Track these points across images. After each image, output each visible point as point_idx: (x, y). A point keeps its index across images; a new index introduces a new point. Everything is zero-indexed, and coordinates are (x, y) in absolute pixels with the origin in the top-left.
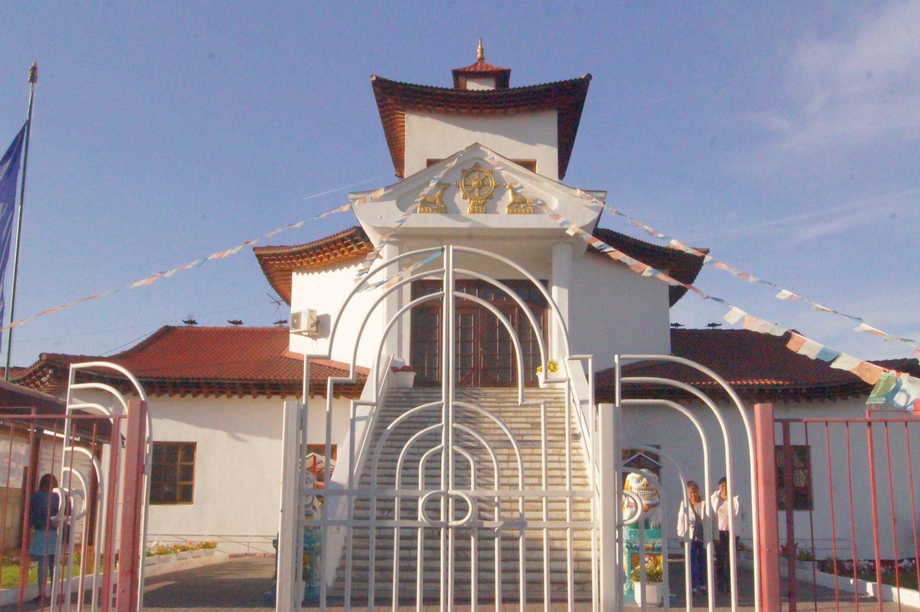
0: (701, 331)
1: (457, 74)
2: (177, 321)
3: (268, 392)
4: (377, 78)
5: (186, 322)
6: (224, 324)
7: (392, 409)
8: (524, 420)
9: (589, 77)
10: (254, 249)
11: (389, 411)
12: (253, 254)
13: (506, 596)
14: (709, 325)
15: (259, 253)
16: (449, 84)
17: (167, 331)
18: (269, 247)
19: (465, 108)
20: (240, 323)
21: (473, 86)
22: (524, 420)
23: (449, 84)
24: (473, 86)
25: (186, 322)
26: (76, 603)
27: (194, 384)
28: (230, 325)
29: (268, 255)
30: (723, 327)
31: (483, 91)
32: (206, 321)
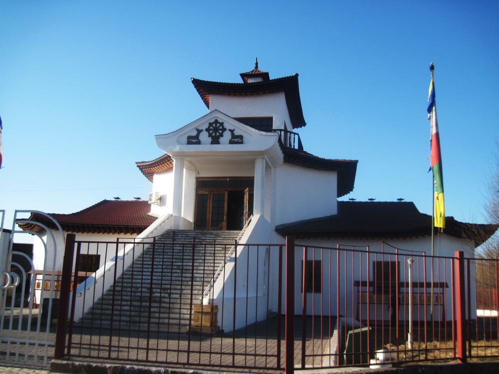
0: (346, 202)
1: (242, 75)
2: (111, 198)
3: (113, 231)
4: (194, 79)
5: (115, 198)
6: (366, 200)
7: (186, 240)
10: (136, 163)
11: (160, 241)
12: (136, 165)
13: (23, 357)
14: (369, 200)
15: (139, 165)
16: (241, 81)
17: (105, 203)
18: (143, 162)
19: (238, 92)
20: (139, 198)
21: (250, 81)
23: (241, 81)
24: (250, 81)
25: (115, 198)
26: (408, 287)
27: (131, 228)
29: (143, 166)
30: (356, 201)
31: (257, 82)
32: (124, 198)
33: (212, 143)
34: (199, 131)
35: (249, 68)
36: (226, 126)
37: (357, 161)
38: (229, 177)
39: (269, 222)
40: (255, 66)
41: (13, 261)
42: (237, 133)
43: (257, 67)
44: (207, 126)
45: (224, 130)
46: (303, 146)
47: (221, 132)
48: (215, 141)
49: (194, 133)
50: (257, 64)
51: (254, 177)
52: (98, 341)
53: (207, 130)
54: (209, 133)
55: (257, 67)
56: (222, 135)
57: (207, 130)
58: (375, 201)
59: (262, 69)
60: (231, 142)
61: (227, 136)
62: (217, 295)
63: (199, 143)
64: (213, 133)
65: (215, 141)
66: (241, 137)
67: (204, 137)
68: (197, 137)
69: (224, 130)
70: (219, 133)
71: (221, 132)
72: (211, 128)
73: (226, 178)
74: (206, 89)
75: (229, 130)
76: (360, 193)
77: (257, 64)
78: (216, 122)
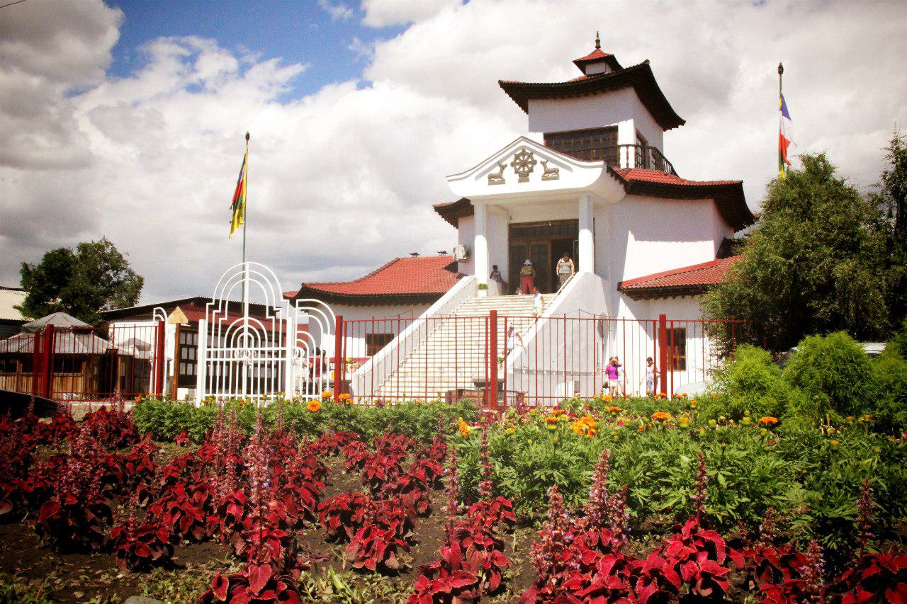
20: (445, 252)
33: (520, 181)
34: (503, 168)
35: (586, 51)
36: (535, 157)
37: (647, 61)
38: (552, 222)
39: (630, 233)
40: (595, 44)
41: (298, 330)
42: (550, 166)
43: (598, 47)
45: (534, 163)
46: (686, 244)
47: (518, 161)
48: (524, 177)
49: (497, 170)
50: (598, 41)
51: (577, 220)
53: (513, 164)
54: (515, 168)
55: (598, 47)
56: (531, 170)
57: (513, 164)
59: (606, 50)
60: (544, 179)
61: (538, 170)
62: (629, 241)
63: (503, 182)
64: (520, 168)
65: (524, 177)
67: (509, 174)
68: (499, 176)
69: (534, 163)
71: (530, 166)
72: (521, 158)
73: (548, 222)
74: (522, 93)
77: (598, 41)
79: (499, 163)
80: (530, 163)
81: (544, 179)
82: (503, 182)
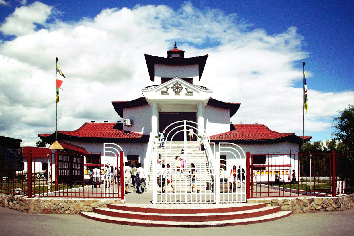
8: (191, 150)
9: (145, 54)
22: (191, 150)
28: (91, 122)
34: (168, 89)
36: (182, 86)
42: (189, 90)
44: (172, 85)
45: (182, 88)
48: (177, 93)
52: (267, 193)
53: (172, 88)
57: (172, 88)
58: (120, 122)
60: (186, 95)
61: (184, 91)
63: (168, 94)
65: (177, 93)
66: (192, 92)
67: (171, 91)
69: (182, 88)
70: (179, 89)
75: (185, 88)
76: (236, 120)
78: (177, 83)
79: (166, 87)
80: (180, 88)
81: (186, 95)
82: (168, 94)
